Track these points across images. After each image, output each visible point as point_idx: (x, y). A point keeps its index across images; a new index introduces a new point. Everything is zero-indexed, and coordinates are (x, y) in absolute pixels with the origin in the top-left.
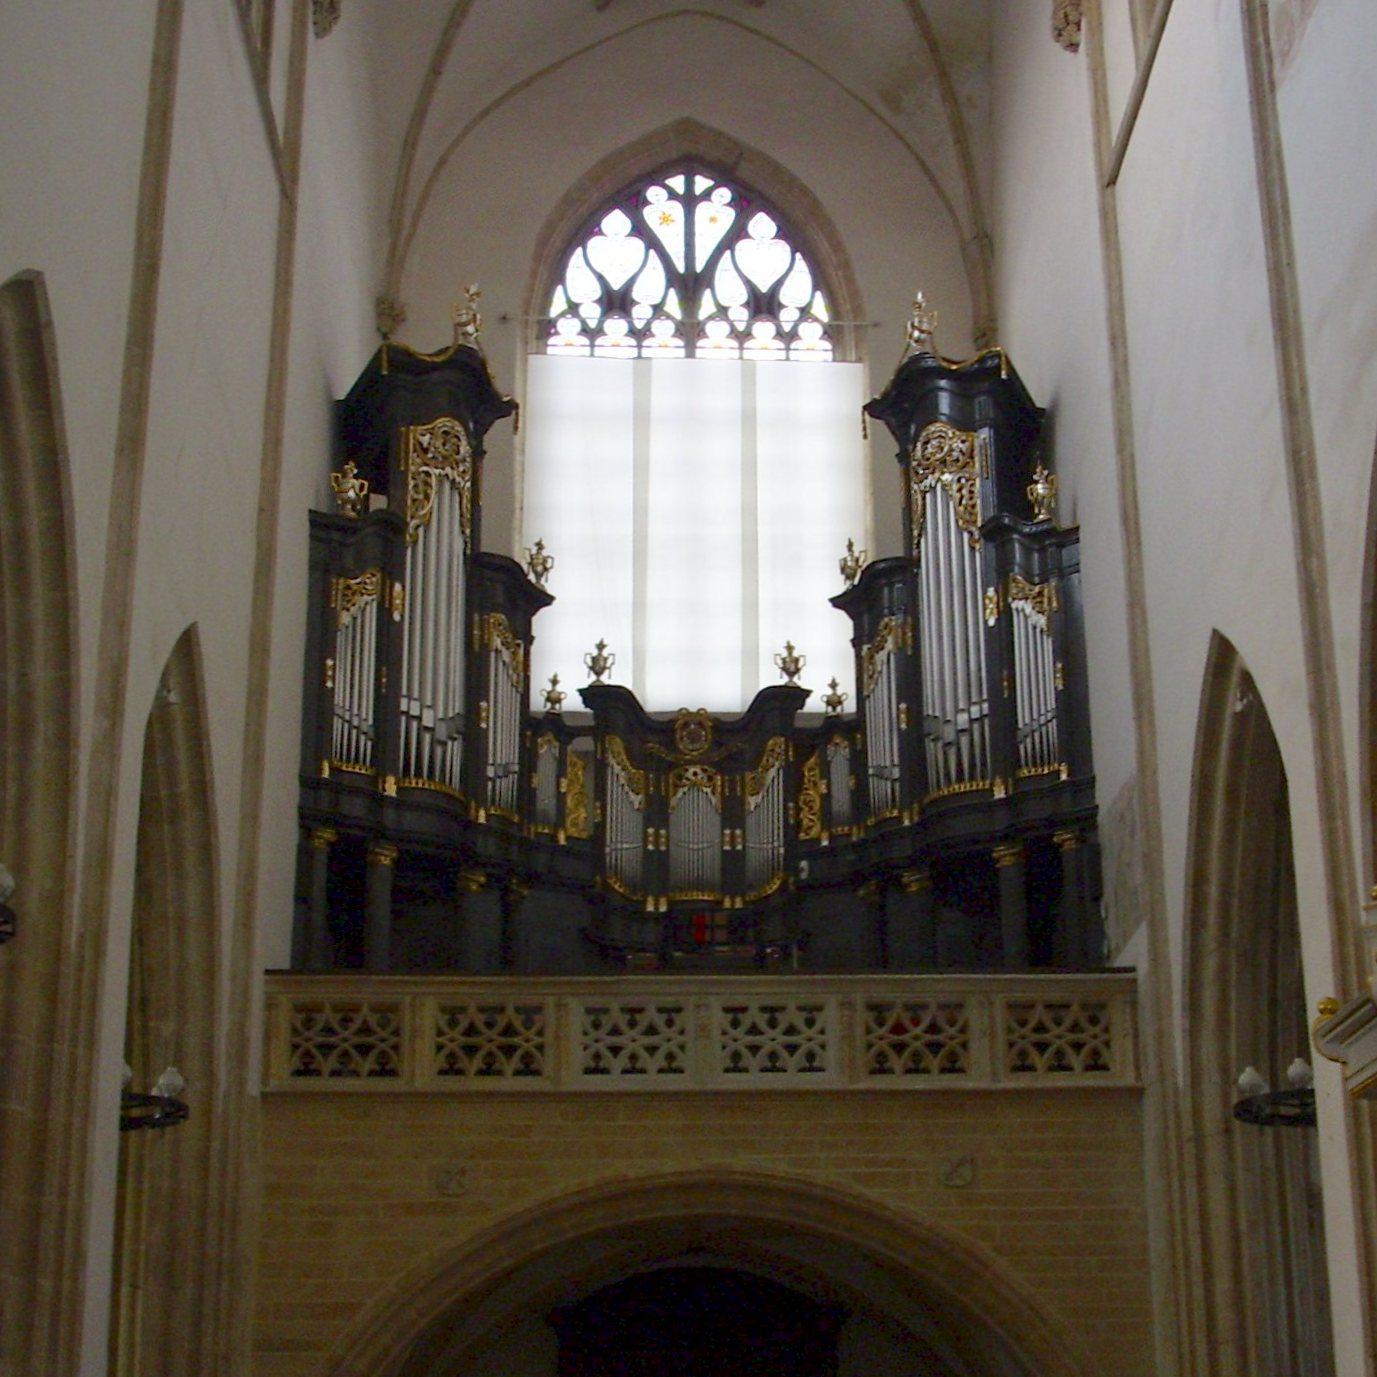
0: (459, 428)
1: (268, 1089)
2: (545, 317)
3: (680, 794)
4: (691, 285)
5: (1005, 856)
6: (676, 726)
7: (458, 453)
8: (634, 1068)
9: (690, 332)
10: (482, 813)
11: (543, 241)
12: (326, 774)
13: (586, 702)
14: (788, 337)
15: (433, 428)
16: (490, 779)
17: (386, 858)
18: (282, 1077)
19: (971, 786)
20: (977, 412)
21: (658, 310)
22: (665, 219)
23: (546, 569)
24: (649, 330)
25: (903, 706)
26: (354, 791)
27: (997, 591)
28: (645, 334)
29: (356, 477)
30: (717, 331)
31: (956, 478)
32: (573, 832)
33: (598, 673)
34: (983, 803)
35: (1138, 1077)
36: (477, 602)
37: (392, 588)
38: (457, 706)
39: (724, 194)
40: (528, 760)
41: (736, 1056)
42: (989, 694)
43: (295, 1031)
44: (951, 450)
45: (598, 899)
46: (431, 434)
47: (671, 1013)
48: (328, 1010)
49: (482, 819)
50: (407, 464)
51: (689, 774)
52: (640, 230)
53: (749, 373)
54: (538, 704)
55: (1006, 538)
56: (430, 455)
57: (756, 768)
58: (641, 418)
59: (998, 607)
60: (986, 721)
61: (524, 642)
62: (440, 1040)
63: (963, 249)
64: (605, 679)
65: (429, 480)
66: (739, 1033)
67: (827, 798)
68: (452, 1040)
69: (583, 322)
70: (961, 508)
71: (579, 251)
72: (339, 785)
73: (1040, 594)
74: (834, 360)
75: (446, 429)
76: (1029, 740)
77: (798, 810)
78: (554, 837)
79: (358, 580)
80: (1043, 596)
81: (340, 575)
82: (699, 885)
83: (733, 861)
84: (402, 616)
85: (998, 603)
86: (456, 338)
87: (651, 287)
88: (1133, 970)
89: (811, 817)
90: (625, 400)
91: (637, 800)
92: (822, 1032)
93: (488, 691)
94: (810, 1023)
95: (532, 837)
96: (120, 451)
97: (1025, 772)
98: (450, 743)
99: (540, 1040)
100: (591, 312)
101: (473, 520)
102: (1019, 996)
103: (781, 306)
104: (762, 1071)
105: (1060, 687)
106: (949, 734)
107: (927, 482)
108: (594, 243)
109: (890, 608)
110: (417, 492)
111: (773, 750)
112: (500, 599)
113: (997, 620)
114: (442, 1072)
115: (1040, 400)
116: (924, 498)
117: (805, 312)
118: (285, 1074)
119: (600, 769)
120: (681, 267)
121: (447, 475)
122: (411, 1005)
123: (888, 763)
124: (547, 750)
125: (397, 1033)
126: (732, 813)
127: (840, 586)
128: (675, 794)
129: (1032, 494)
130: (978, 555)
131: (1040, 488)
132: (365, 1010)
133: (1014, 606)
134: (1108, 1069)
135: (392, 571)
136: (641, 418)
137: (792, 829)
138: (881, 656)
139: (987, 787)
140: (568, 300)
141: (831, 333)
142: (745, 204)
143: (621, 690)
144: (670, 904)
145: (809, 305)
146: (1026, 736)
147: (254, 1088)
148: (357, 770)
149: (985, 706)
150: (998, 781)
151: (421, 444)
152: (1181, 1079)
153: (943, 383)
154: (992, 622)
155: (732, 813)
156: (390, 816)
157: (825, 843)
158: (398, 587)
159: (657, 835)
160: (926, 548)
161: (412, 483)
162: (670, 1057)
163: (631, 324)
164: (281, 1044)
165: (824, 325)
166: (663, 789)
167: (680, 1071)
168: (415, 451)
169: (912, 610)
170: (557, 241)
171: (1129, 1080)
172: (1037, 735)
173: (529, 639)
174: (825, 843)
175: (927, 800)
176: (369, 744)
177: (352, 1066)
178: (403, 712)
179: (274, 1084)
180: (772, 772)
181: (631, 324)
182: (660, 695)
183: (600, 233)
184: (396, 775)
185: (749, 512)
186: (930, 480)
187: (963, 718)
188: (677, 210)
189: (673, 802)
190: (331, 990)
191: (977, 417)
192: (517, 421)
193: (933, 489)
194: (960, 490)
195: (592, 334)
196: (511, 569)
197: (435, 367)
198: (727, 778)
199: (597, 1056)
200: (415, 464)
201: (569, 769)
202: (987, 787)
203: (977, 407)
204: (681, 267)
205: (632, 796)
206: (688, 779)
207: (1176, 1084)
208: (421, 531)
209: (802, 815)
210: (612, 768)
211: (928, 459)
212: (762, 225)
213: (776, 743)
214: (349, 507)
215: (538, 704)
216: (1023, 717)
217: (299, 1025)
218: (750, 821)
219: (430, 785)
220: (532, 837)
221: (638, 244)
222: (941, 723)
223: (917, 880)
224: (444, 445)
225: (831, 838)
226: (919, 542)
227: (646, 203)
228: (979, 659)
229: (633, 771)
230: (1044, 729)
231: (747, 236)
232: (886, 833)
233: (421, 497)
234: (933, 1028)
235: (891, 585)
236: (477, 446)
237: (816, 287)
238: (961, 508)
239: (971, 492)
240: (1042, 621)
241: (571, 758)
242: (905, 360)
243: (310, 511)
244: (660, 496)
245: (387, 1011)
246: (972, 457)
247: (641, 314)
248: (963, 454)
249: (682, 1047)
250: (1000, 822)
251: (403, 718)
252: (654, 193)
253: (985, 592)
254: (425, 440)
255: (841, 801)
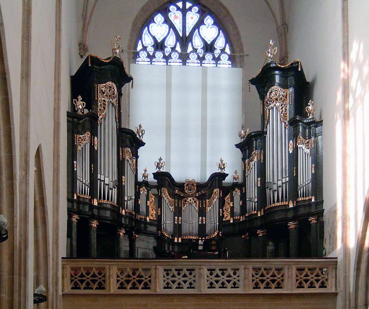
0: (115, 86)
1: (63, 293)
2: (136, 51)
3: (185, 206)
4: (185, 40)
5: (292, 225)
6: (185, 185)
7: (114, 94)
8: (179, 287)
9: (184, 58)
10: (124, 211)
11: (134, 24)
12: (75, 198)
13: (155, 178)
14: (217, 60)
15: (106, 85)
16: (126, 201)
17: (95, 224)
18: (68, 290)
19: (282, 204)
20: (289, 82)
21: (173, 49)
22: (176, 17)
23: (142, 134)
24: (170, 56)
25: (259, 179)
26: (85, 203)
27: (293, 142)
28: (169, 58)
29: (81, 101)
30: (193, 57)
31: (281, 104)
32: (151, 218)
33: (159, 168)
34: (285, 209)
35: (336, 290)
36: (121, 143)
37: (94, 138)
38: (116, 178)
39: (196, 9)
40: (137, 195)
41: (211, 284)
42: (288, 175)
43: (72, 276)
44: (280, 95)
45: (160, 239)
46: (105, 87)
47: (191, 271)
48: (94, 269)
49: (124, 213)
50: (97, 97)
51: (189, 200)
52: (167, 21)
53: (205, 72)
54: (140, 179)
55: (297, 124)
56: (105, 95)
57: (210, 198)
58: (169, 86)
59: (293, 147)
60: (287, 183)
61: (135, 157)
62: (118, 278)
63: (277, 29)
64: (162, 170)
65: (105, 103)
66: (212, 277)
67: (232, 208)
68: (122, 279)
69: (148, 53)
70: (282, 115)
71: (146, 28)
72: (79, 201)
73: (308, 142)
74: (232, 67)
75: (110, 86)
76: (302, 189)
77: (223, 211)
78: (145, 219)
79: (83, 136)
80: (309, 143)
81: (77, 134)
82: (191, 234)
83: (202, 227)
84: (98, 148)
85: (293, 146)
86: (113, 54)
87: (171, 41)
88: (336, 258)
89: (227, 214)
90: (164, 80)
91: (172, 208)
92: (238, 277)
93: (125, 173)
94: (235, 274)
95: (139, 219)
96: (22, 78)
97: (300, 199)
98: (114, 189)
99: (150, 279)
100: (151, 50)
101: (119, 119)
102: (300, 266)
103: (215, 49)
104: (219, 288)
105: (313, 172)
106: (275, 187)
107: (271, 106)
108: (152, 25)
109: (256, 148)
110: (101, 107)
111: (215, 193)
112: (128, 143)
113: (293, 151)
114: (119, 288)
115: (309, 79)
116: (269, 111)
117: (223, 51)
118: (70, 288)
119: (159, 199)
120: (181, 34)
121: (111, 101)
122: (109, 268)
123: (254, 197)
124: (143, 191)
125: (104, 276)
126: (202, 212)
127: (239, 141)
128: (184, 206)
129: (307, 110)
130: (287, 129)
131: (310, 108)
132: (94, 269)
133: (299, 146)
134: (327, 287)
135: (94, 133)
136: (169, 86)
137: (221, 218)
138: (253, 163)
139: (287, 204)
140: (143, 46)
141: (231, 58)
142: (203, 13)
143: (167, 173)
144: (182, 240)
145: (224, 48)
146: (301, 188)
147: (60, 293)
148: (85, 197)
149: (287, 179)
150: (291, 202)
151: (102, 91)
152: (352, 290)
153: (277, 72)
154: (291, 152)
155: (202, 212)
156: (95, 212)
157: (232, 221)
158: (96, 138)
159: (178, 219)
160: (269, 129)
161: (99, 104)
162: (191, 284)
163: (164, 54)
164: (68, 279)
165: (229, 55)
166: (180, 204)
167: (194, 288)
168: (100, 93)
169: (263, 148)
170: (140, 25)
171: (333, 290)
172: (304, 188)
173: (137, 157)
174: (232, 221)
175: (266, 208)
176: (89, 189)
177: (90, 286)
178: (99, 179)
179: (66, 291)
180: (215, 200)
181: (164, 54)
182: (178, 176)
183: (154, 22)
184: (97, 199)
185: (204, 119)
186: (272, 105)
187: (280, 183)
188: (179, 14)
189: (183, 209)
190: (83, 264)
191: (289, 84)
192: (132, 84)
193: (272, 108)
194: (282, 109)
195: (151, 57)
196: (131, 133)
197: (106, 64)
198: (200, 201)
199: (168, 284)
200: (100, 98)
201: (150, 198)
202: (287, 204)
203: (289, 81)
204: (181, 34)
205: (170, 207)
206: (188, 202)
207: (350, 291)
208: (103, 120)
209: (224, 213)
210: (164, 198)
211: (272, 98)
212: (209, 20)
213: (216, 190)
214: (80, 110)
215: (140, 179)
216: (300, 182)
217: (73, 274)
218: (208, 214)
219: (108, 202)
220: (139, 219)
221: (166, 27)
222: (272, 184)
223: (262, 233)
224: (110, 91)
225: (234, 220)
226: (267, 126)
227: (169, 11)
228: (286, 164)
229: (171, 199)
230: (307, 185)
231: (204, 24)
232: (252, 218)
233: (103, 108)
234: (273, 276)
235: (256, 140)
236: (120, 92)
237: (226, 42)
238: (282, 115)
239: (286, 109)
240: (308, 151)
241: (151, 195)
242: (265, 64)
243: (67, 112)
244: (174, 113)
245: (101, 271)
246: (286, 97)
247: (168, 50)
248: (284, 97)
249: (194, 281)
250: (290, 215)
251: (99, 181)
252: (172, 8)
253: (289, 142)
254: (103, 89)
255: (237, 209)
